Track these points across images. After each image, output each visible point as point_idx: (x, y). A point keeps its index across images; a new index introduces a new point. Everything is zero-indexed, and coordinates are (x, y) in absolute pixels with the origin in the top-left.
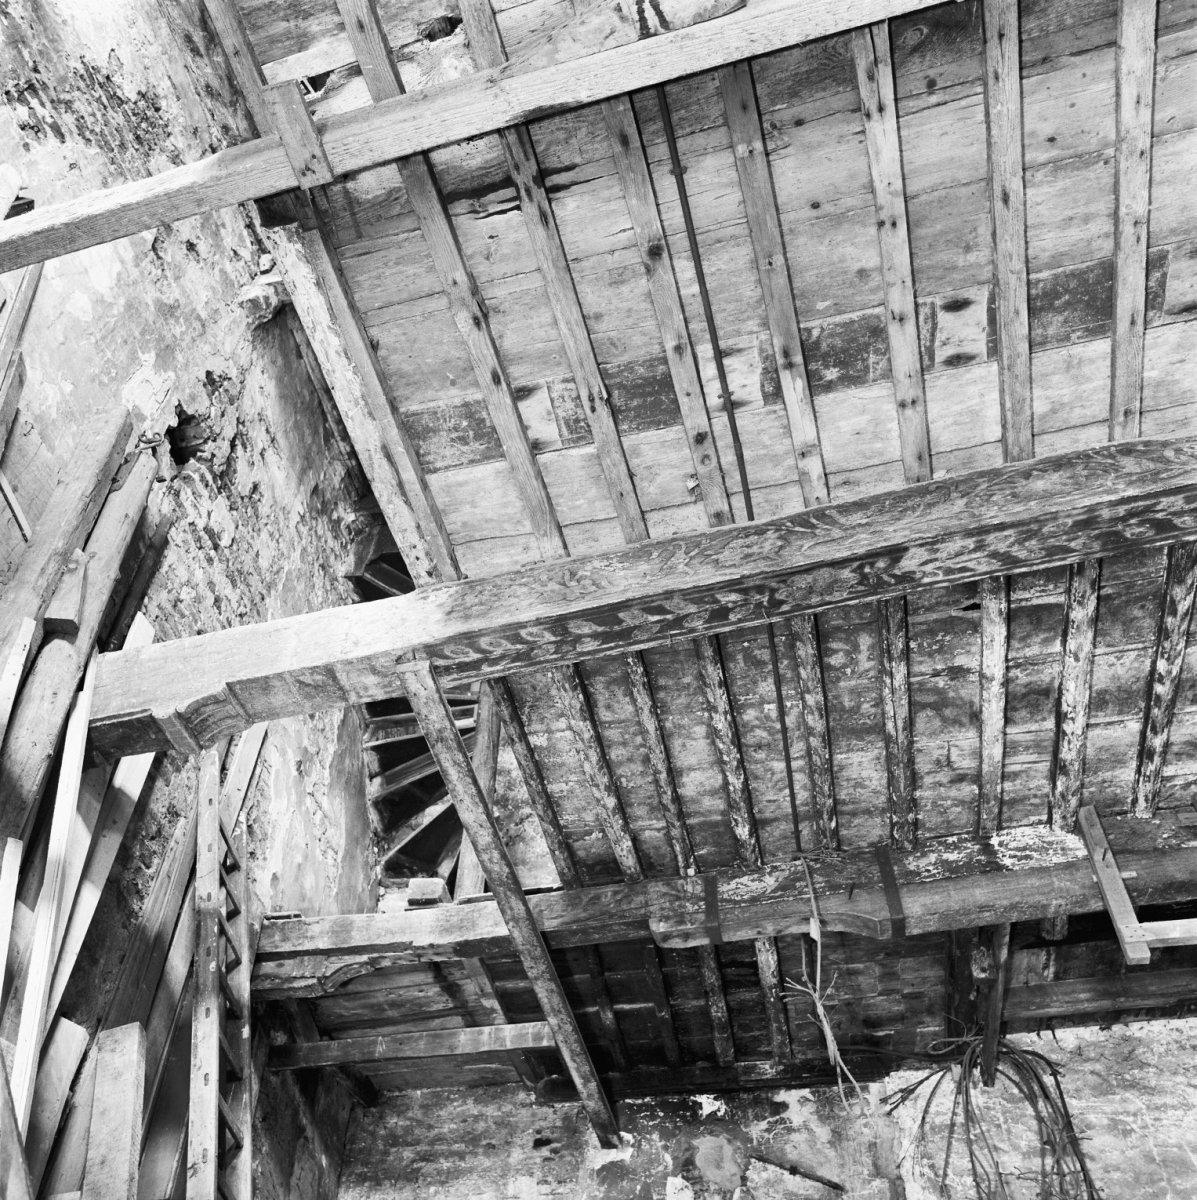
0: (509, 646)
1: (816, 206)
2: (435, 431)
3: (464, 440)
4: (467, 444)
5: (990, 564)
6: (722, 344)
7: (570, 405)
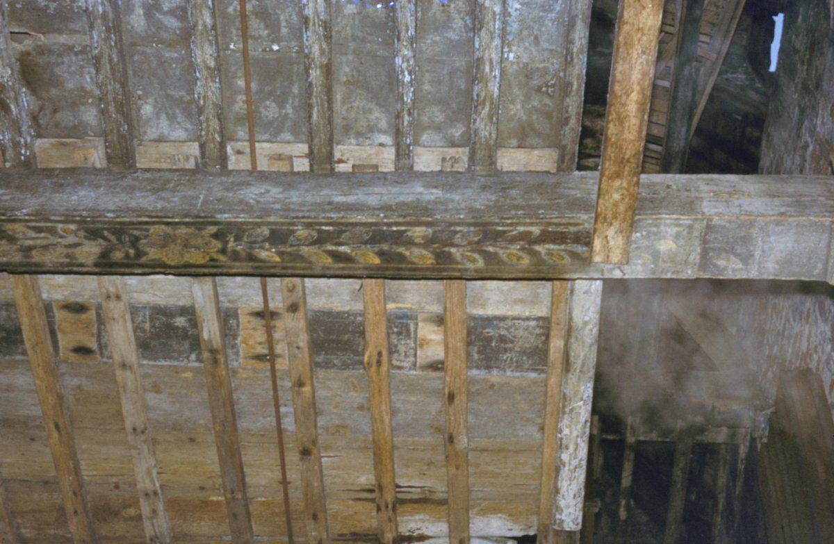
0: (501, 252)
1: (192, 440)
2: (523, 352)
3: (502, 339)
4: (501, 336)
5: (14, 230)
6: (268, 365)
7: (402, 348)
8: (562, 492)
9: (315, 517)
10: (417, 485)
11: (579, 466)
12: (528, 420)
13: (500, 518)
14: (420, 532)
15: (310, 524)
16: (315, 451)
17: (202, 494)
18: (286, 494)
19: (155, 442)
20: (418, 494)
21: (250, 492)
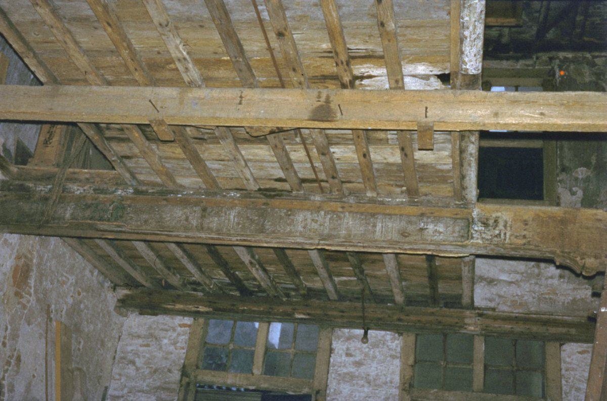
1: (201, 26)
8: (465, 53)
9: (294, 70)
10: (362, 48)
11: (478, 37)
12: (439, 8)
13: (424, 65)
14: (369, 74)
15: (292, 73)
16: (287, 34)
17: (217, 57)
18: (272, 55)
19: (177, 28)
20: (364, 53)
21: (248, 55)
